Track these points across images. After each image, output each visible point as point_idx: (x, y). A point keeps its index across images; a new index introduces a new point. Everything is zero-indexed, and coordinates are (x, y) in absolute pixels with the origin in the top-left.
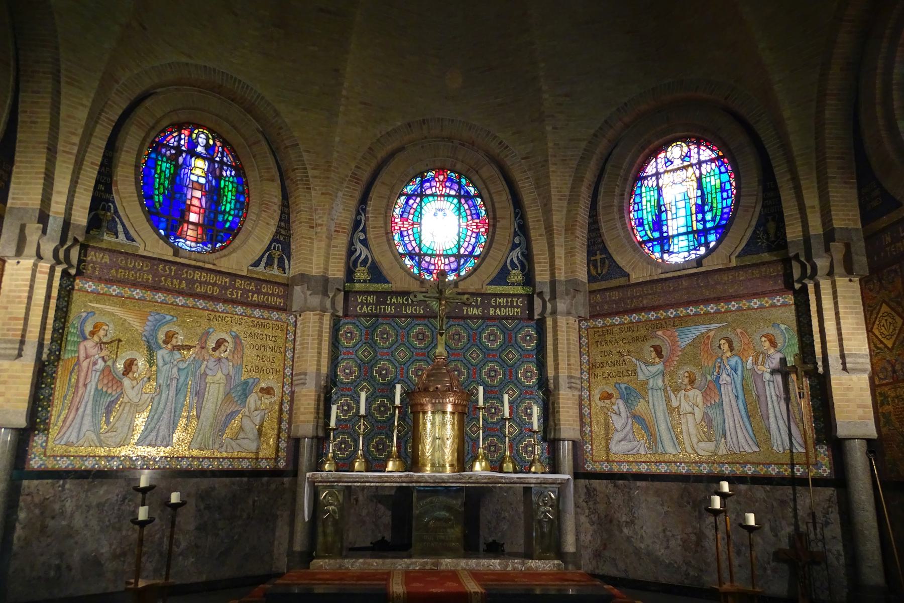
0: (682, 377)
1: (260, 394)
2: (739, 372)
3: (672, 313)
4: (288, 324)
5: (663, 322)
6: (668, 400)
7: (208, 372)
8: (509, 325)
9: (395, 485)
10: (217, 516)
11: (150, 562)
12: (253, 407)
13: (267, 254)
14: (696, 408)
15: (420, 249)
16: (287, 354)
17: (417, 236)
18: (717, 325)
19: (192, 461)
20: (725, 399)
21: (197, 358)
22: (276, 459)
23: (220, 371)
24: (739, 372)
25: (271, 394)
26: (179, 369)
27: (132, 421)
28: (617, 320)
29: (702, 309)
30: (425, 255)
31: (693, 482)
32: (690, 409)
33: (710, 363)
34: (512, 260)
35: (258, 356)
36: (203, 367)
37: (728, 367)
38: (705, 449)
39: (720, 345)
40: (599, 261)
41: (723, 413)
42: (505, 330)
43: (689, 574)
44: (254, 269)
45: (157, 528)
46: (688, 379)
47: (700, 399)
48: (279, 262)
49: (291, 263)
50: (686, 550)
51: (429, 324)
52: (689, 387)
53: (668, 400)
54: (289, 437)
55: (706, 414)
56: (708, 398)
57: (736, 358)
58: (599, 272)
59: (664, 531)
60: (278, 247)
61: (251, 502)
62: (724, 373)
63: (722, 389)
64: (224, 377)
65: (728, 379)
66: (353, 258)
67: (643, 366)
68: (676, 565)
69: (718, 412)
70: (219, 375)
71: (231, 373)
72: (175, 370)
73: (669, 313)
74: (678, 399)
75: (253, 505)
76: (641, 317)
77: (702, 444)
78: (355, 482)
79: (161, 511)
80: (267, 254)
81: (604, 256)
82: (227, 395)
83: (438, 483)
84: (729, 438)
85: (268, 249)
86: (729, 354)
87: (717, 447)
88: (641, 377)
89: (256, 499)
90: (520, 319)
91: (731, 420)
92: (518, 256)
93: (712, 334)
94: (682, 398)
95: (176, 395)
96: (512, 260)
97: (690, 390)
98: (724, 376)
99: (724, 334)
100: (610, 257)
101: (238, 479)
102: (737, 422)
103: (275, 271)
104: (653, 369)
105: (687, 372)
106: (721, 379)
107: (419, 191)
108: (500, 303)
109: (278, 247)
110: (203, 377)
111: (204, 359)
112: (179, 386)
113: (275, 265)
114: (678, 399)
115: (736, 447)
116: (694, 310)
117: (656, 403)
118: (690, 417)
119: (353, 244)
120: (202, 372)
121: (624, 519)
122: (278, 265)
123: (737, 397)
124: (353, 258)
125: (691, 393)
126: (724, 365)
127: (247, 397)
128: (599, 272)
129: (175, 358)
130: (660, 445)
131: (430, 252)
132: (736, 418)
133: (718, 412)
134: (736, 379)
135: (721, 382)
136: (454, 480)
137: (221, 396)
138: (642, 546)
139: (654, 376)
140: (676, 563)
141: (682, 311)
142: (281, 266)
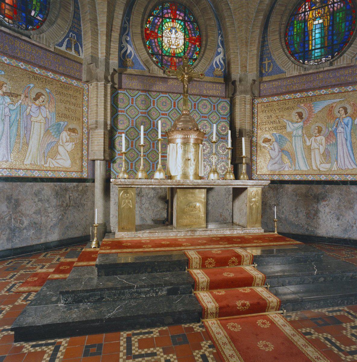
0: (314, 128)
1: (69, 133)
2: (349, 126)
3: (311, 93)
4: (83, 89)
5: (305, 99)
6: (304, 142)
7: (32, 114)
8: (214, 100)
9: (168, 186)
10: (47, 206)
11: (4, 234)
12: (65, 140)
13: (67, 39)
14: (321, 146)
15: (162, 52)
16: (84, 108)
17: (160, 43)
18: (338, 100)
19: (26, 172)
20: (339, 141)
21: (23, 104)
22: (82, 172)
23: (40, 115)
24: (349, 126)
25: (76, 133)
26: (10, 109)
27: (172, 352)
28: (276, 98)
29: (330, 91)
30: (166, 55)
31: (315, 184)
32: (317, 147)
33: (332, 122)
34: (216, 62)
35: (65, 108)
36: (28, 110)
37: (343, 123)
38: (324, 167)
39: (339, 111)
40: (267, 64)
41: (337, 149)
42: (212, 103)
43: (308, 229)
44: (59, 48)
45: (6, 214)
46: (317, 130)
47: (324, 141)
48: (75, 47)
49: (83, 50)
50: (308, 218)
51: (169, 97)
52: (318, 135)
53: (304, 142)
54: (88, 160)
55: (326, 149)
56: (329, 141)
57: (348, 118)
58: (267, 71)
59: (296, 209)
60: (74, 36)
61: (67, 196)
62: (340, 127)
63: (338, 135)
64: (44, 119)
65: (342, 130)
66: (123, 51)
67: (290, 124)
68: (301, 225)
69: (334, 148)
70: (40, 117)
71: (48, 116)
72: (7, 110)
73: (309, 94)
74: (310, 141)
75: (70, 199)
76: (291, 96)
77: (323, 165)
78: (142, 185)
79: (8, 203)
80: (67, 39)
81: (269, 61)
82: (47, 131)
83: (195, 185)
84: (339, 162)
85: (67, 36)
86: (344, 116)
87: (332, 166)
88: (289, 130)
89: (71, 195)
90: (220, 97)
91: (341, 152)
92: (219, 60)
93: (334, 105)
94: (313, 140)
95: (10, 127)
96: (216, 62)
97: (317, 136)
98: (340, 128)
99: (343, 105)
100: (274, 62)
101: (58, 183)
102: (345, 153)
103: (73, 53)
104: (296, 125)
105: (318, 126)
106: (338, 130)
107: (161, 14)
108: (209, 87)
109: (74, 36)
110: (29, 118)
111: (28, 105)
112: (12, 121)
113: (73, 49)
114: (310, 141)
115: (343, 166)
116: (325, 92)
117: (297, 144)
118: (317, 151)
119: (122, 43)
120: (28, 113)
121: (273, 203)
122: (74, 49)
123: (346, 140)
124: (123, 51)
125: (318, 138)
126: (340, 122)
127: (60, 134)
128: (267, 71)
129: (6, 101)
130: (297, 165)
131: (167, 54)
132: (345, 151)
133: (334, 148)
134: (347, 130)
135: (337, 132)
136: (205, 184)
137: (43, 132)
138: (283, 216)
139: (297, 129)
140: (302, 224)
141: (317, 92)
142: (77, 50)
